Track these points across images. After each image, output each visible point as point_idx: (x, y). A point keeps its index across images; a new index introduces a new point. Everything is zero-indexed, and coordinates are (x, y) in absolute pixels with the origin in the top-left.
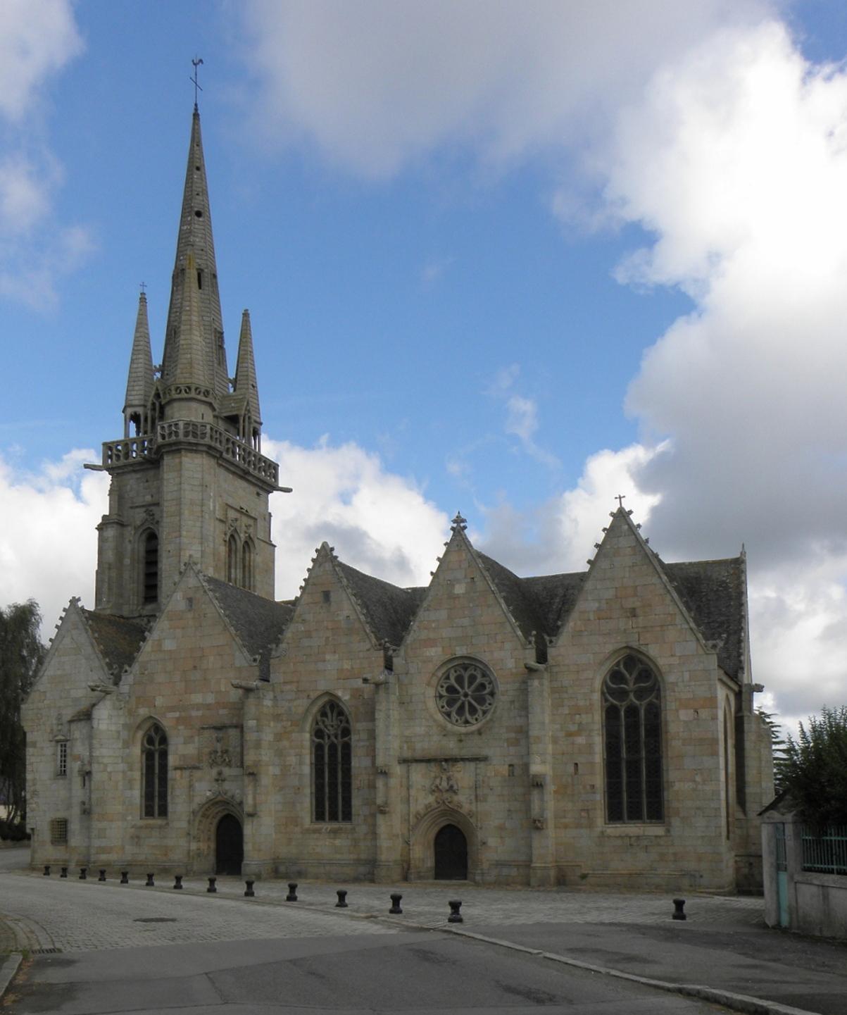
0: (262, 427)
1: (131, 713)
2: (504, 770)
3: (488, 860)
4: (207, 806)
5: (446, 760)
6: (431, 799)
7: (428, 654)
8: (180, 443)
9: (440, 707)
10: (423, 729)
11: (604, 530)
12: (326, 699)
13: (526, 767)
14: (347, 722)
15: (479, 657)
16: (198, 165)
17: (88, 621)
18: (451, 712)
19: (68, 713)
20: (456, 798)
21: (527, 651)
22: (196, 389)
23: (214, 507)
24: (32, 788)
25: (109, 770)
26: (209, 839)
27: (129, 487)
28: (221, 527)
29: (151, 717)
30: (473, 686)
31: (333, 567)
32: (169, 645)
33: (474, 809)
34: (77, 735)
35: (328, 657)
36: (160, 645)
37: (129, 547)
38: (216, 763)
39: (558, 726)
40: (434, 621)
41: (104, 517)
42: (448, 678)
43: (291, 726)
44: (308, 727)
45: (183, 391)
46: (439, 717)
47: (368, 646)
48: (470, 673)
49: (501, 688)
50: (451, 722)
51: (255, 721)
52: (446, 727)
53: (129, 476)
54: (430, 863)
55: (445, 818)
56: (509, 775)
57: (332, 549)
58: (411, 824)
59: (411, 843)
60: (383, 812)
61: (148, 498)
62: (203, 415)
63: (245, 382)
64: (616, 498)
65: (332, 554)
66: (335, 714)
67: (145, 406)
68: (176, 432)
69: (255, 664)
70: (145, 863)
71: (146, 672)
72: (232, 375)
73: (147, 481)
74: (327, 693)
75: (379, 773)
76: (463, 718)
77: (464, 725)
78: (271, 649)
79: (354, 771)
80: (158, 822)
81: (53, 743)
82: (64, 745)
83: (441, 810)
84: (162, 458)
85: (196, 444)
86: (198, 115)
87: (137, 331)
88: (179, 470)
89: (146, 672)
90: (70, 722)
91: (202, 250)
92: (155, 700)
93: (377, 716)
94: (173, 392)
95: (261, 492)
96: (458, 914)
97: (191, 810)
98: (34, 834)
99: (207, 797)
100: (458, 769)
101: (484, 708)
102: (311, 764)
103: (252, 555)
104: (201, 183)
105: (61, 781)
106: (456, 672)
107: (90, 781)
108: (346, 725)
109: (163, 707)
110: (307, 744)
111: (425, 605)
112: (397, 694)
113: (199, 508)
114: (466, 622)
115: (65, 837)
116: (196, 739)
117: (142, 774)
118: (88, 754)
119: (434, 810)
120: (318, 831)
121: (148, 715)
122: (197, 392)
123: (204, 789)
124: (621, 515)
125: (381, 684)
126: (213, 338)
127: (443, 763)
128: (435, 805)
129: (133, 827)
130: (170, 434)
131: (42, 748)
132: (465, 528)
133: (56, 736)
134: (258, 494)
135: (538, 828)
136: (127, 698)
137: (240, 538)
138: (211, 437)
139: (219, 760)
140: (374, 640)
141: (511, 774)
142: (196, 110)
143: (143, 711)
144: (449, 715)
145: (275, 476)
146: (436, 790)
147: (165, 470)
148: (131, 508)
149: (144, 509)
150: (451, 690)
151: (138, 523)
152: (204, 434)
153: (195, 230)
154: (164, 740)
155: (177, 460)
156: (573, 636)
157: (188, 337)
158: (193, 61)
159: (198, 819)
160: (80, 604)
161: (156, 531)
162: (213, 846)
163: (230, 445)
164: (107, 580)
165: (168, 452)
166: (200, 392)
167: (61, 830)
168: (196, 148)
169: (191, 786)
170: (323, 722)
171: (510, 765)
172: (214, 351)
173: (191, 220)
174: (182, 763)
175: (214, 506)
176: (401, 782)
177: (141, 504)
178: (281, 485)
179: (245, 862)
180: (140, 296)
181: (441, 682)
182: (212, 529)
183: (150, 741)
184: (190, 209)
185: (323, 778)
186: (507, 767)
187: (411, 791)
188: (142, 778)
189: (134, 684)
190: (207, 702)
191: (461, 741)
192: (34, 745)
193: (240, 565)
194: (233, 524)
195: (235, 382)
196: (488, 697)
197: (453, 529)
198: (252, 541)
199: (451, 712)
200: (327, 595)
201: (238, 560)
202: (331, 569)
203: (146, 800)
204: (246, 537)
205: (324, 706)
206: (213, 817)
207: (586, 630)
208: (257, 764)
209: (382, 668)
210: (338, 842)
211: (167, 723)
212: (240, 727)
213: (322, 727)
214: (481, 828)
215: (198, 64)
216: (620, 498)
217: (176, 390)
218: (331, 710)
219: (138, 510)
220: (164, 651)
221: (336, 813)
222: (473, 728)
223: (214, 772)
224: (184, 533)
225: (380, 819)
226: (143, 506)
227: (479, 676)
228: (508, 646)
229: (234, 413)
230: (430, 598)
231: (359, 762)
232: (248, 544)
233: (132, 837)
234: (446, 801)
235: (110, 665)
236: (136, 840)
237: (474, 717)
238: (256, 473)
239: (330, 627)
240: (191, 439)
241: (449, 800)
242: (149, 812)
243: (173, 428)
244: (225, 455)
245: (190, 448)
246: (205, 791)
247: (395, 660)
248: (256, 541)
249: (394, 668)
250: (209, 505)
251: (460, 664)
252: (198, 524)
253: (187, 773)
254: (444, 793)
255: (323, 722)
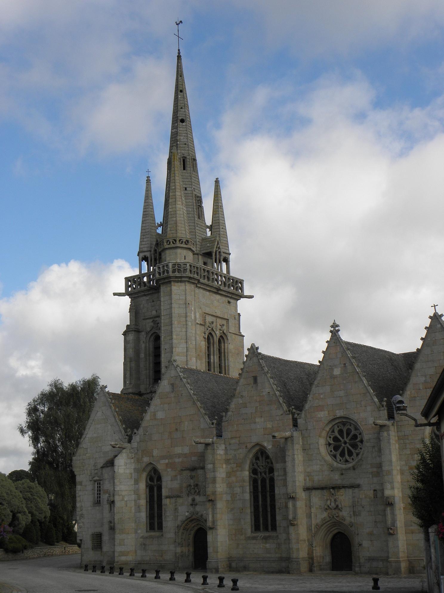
0: (230, 256)
1: (138, 461)
2: (371, 493)
3: (363, 557)
4: (186, 522)
5: (333, 488)
6: (325, 515)
7: (319, 416)
8: (170, 277)
9: (329, 452)
10: (318, 466)
11: (426, 328)
12: (257, 448)
13: (383, 491)
14: (272, 463)
15: (351, 417)
16: (181, 89)
17: (112, 400)
18: (336, 454)
19: (101, 462)
20: (341, 514)
21: (381, 412)
22: (180, 240)
23: (195, 317)
24: (81, 513)
25: (125, 500)
26: (189, 545)
27: (142, 306)
28: (202, 328)
29: (151, 463)
30: (350, 437)
31: (258, 360)
32: (160, 415)
33: (353, 521)
34: (106, 476)
35: (257, 420)
36: (155, 415)
37: (143, 346)
38: (191, 493)
39: (403, 463)
40: (322, 394)
41: (128, 326)
42: (333, 431)
43: (237, 467)
44: (247, 467)
45: (171, 243)
46: (329, 458)
47: (281, 412)
48: (347, 427)
49: (366, 437)
50: (336, 462)
51: (212, 465)
52: (333, 465)
53: (142, 299)
54: (328, 559)
55: (336, 527)
56: (374, 497)
57: (257, 348)
58: (313, 532)
59: (314, 545)
60: (293, 525)
61: (154, 313)
62: (185, 256)
63: (218, 227)
64: (432, 306)
65: (257, 351)
66: (264, 458)
67: (150, 251)
68: (167, 270)
69: (213, 426)
70: (149, 562)
71: (147, 434)
72: (209, 221)
73: (153, 301)
74: (257, 444)
75: (289, 498)
76: (344, 458)
77: (344, 463)
78: (222, 416)
79: (277, 497)
80: (157, 534)
81: (92, 482)
82: (98, 483)
83: (333, 522)
84: (160, 286)
85: (181, 277)
86: (181, 56)
87: (145, 202)
88: (170, 294)
89: (147, 434)
90: (102, 467)
91: (185, 144)
92: (153, 452)
93: (287, 460)
94: (165, 244)
95: (231, 300)
96: (237, 586)
97: (177, 526)
98: (82, 543)
99: (187, 516)
100: (341, 494)
101: (357, 451)
102: (250, 492)
103: (226, 344)
104: (184, 100)
105: (97, 508)
106: (338, 427)
107: (114, 506)
108: (271, 465)
109: (158, 456)
110: (247, 479)
111: (316, 383)
112: (301, 444)
113: (184, 319)
114: (342, 393)
115: (100, 546)
116: (179, 477)
117: (147, 502)
118: (113, 489)
119: (327, 522)
120: (254, 538)
121: (149, 462)
122: (181, 242)
123: (184, 512)
124: (436, 318)
125: (289, 437)
126: (194, 201)
127: (331, 490)
128: (328, 519)
129: (141, 538)
130: (164, 272)
131: (86, 486)
132: (338, 330)
133: (94, 477)
134: (229, 302)
135: (391, 534)
136: (136, 451)
137: (216, 334)
138: (190, 271)
139: (193, 491)
140: (285, 408)
141: (375, 496)
142: (179, 53)
143: (146, 460)
144: (335, 456)
145: (242, 289)
146: (327, 508)
147: (162, 295)
148: (144, 319)
149: (151, 320)
150: (336, 439)
151: (149, 329)
152: (185, 270)
153: (180, 132)
154: (159, 479)
155: (169, 288)
156: (410, 401)
157: (174, 206)
158: (176, 22)
159: (181, 531)
160: (107, 390)
161: (159, 334)
162: (191, 549)
163: (206, 274)
164: (129, 369)
165: (163, 283)
166: (182, 242)
167: (97, 539)
168: (180, 78)
169: (176, 509)
170: (257, 464)
171: (374, 490)
172: (195, 210)
173: (177, 125)
174: (170, 494)
175: (195, 315)
176: (306, 503)
177: (149, 317)
178: (246, 293)
179: (208, 560)
180: (146, 179)
181: (329, 434)
182: (194, 332)
183: (151, 479)
184: (176, 118)
185: (258, 502)
186: (372, 492)
187: (312, 509)
188: (147, 505)
189: (140, 442)
190: (185, 453)
191: (342, 474)
192: (81, 484)
193: (216, 352)
194: (210, 326)
195: (211, 228)
196: (359, 444)
197: (331, 332)
198: (226, 336)
199: (336, 454)
200: (255, 379)
201: (215, 349)
202: (257, 361)
203: (150, 519)
204: (220, 333)
205: (257, 453)
206: (191, 530)
207: (418, 396)
208: (214, 493)
209: (291, 427)
210: (268, 546)
211: (160, 467)
212: (203, 468)
213: (256, 466)
214: (358, 534)
215: (179, 24)
216: (435, 306)
217: (167, 243)
218: (261, 455)
219: (148, 321)
220: (158, 419)
221: (259, 526)
222: (350, 465)
223: (190, 499)
224: (174, 337)
225: (291, 529)
226: (151, 318)
227: (353, 429)
228: (369, 408)
229: (209, 251)
230: (319, 378)
231: (278, 491)
232: (222, 339)
233: (141, 545)
234: (335, 516)
235: (125, 430)
236: (144, 546)
237: (351, 458)
238: (226, 289)
239: (258, 400)
240: (177, 274)
241: (337, 515)
242: (151, 527)
243: (165, 268)
244: (202, 280)
245: (178, 280)
246: (185, 512)
247: (299, 421)
248: (229, 335)
249: (298, 426)
250: (192, 316)
251: (340, 422)
252: (184, 330)
253: (173, 500)
254: (333, 511)
255: (257, 464)
